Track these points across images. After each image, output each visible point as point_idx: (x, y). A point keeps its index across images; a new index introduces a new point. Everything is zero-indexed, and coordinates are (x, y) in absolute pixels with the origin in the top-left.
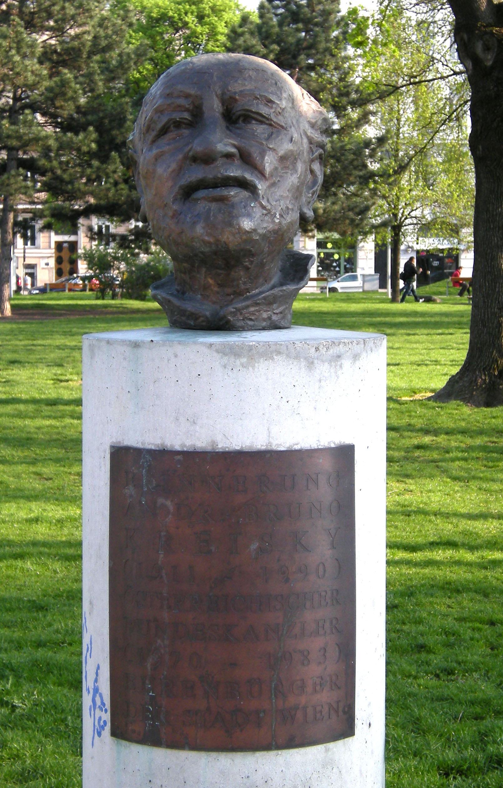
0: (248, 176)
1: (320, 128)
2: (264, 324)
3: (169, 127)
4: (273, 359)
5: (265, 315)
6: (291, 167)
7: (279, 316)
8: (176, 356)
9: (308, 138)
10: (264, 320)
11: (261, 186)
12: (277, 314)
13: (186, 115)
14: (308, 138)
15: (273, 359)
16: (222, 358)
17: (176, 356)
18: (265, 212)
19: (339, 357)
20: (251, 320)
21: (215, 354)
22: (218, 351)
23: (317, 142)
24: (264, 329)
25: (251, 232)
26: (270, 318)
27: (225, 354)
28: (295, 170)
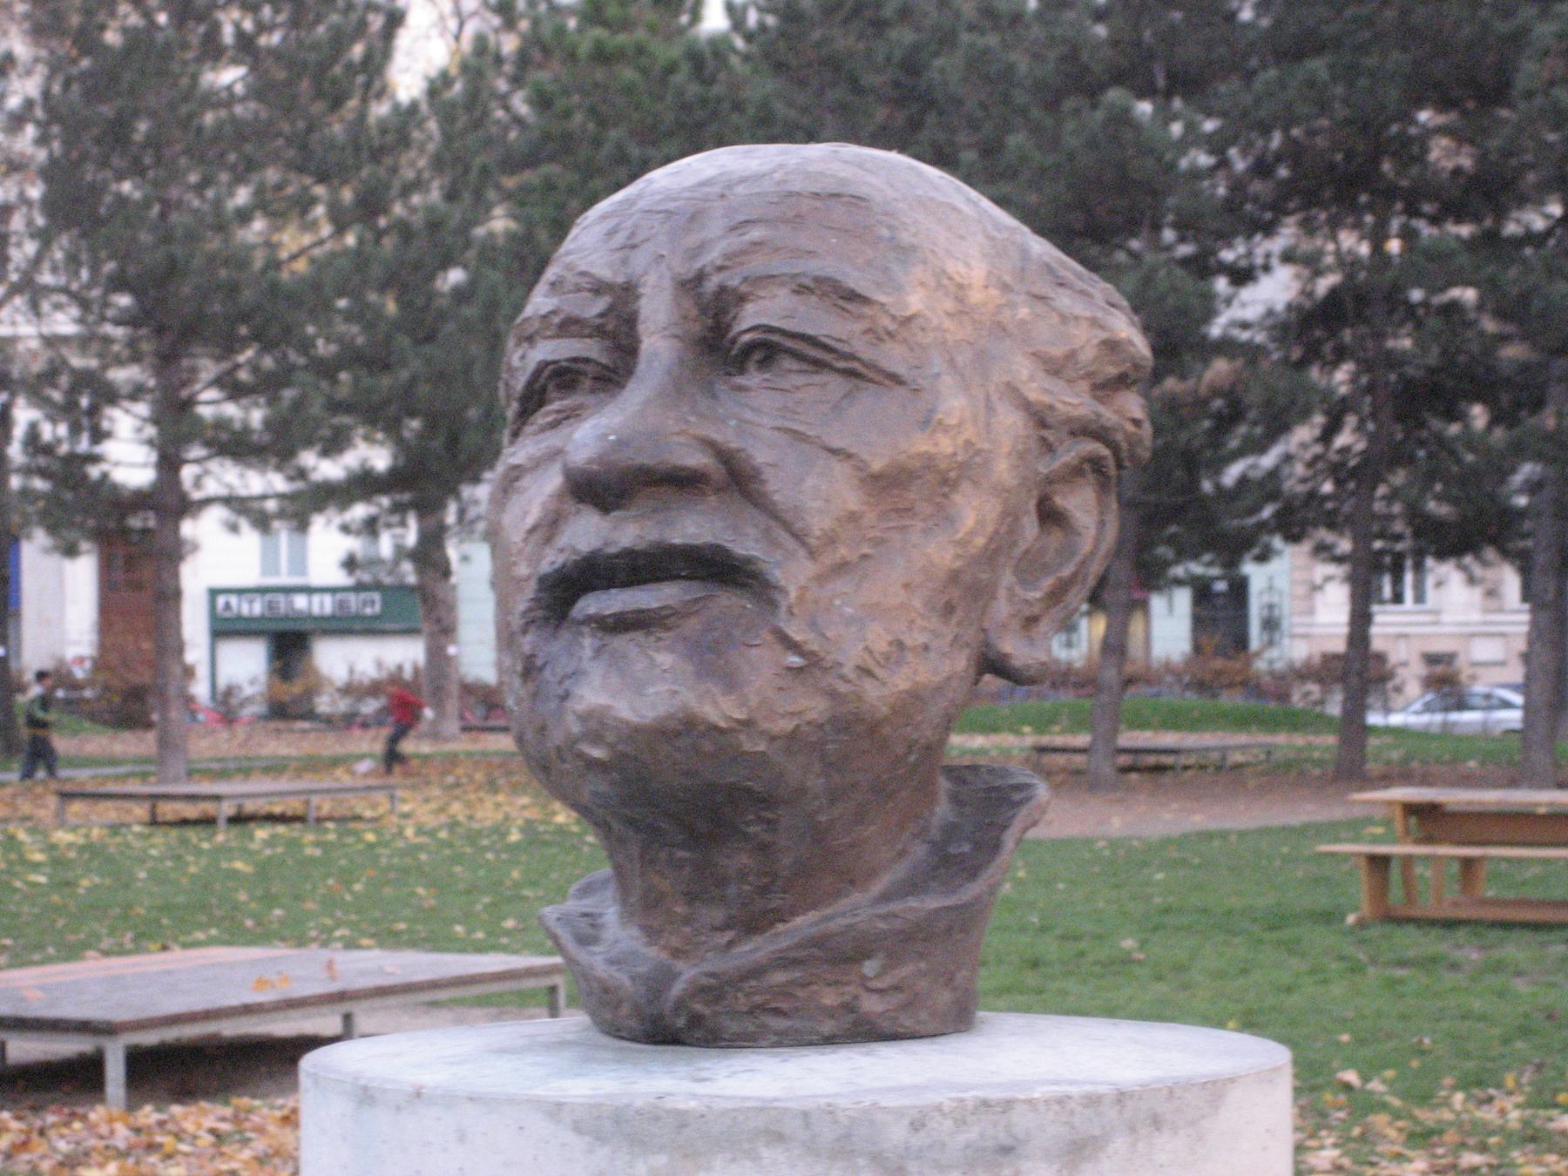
0: (746, 544)
1: (1089, 375)
2: (827, 1027)
3: (544, 390)
4: (756, 1158)
5: (829, 998)
6: (924, 508)
7: (896, 999)
8: (462, 1138)
9: (1027, 406)
10: (830, 1013)
11: (792, 574)
12: (881, 991)
13: (591, 348)
14: (1027, 406)
15: (756, 1158)
16: (591, 1151)
17: (462, 1138)
18: (795, 660)
19: (1006, 1150)
20: (778, 1012)
21: (570, 1137)
22: (578, 1128)
23: (1069, 420)
24: (830, 1041)
25: (731, 730)
26: (848, 1007)
27: (600, 1138)
28: (944, 517)
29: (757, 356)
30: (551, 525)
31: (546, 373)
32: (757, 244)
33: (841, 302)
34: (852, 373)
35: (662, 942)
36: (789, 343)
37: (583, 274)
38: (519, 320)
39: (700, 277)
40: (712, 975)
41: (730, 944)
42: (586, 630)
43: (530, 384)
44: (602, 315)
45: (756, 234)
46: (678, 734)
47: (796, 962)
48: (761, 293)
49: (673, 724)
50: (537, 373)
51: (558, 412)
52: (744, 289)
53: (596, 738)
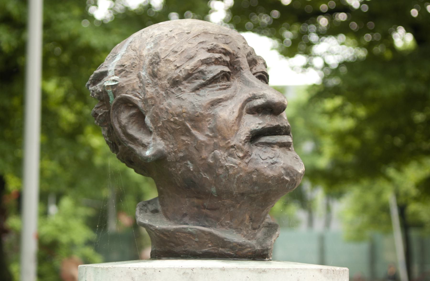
35: (242, 233)
42: (276, 146)
51: (227, 85)
53: (288, 174)
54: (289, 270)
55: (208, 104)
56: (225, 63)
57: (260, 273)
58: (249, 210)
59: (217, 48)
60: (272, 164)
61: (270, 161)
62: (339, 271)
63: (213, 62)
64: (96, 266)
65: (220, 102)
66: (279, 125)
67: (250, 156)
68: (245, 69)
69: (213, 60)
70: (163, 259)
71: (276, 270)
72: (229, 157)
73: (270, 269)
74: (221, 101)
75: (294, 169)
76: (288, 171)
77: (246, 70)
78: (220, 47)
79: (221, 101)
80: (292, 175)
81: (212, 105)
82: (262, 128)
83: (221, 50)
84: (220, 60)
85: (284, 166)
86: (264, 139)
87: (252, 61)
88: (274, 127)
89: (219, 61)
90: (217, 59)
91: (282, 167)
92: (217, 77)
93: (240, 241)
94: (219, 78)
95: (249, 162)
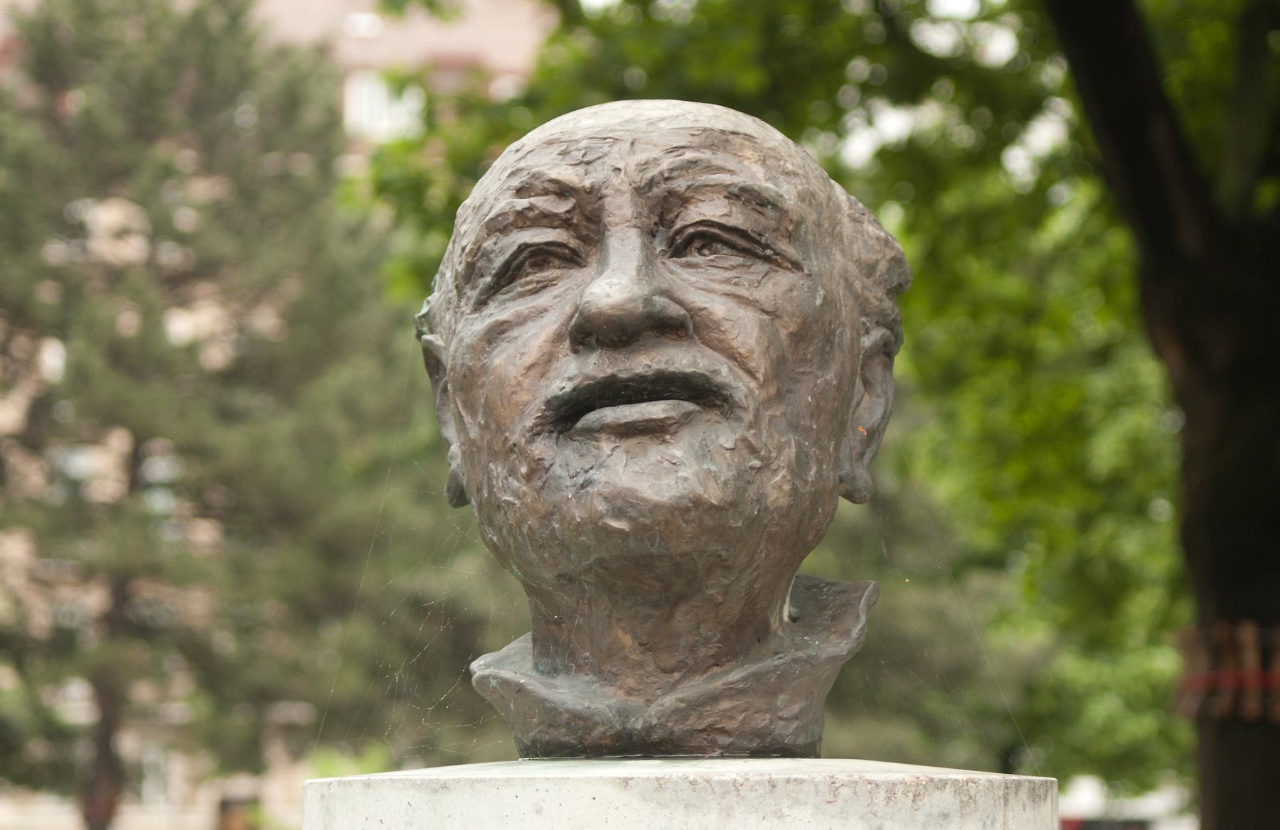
29: (697, 244)
30: (544, 365)
31: (525, 254)
32: (694, 163)
33: (759, 208)
34: (767, 259)
35: (619, 683)
36: (725, 236)
37: (552, 181)
38: (833, 182)
39: (652, 183)
40: (682, 700)
41: (678, 682)
42: (603, 436)
43: (507, 264)
44: (568, 212)
45: (689, 155)
46: (688, 510)
47: (740, 692)
48: (698, 197)
49: (686, 502)
50: (516, 255)
51: (538, 282)
52: (688, 194)
53: (619, 513)
54: (508, 781)
55: (481, 340)
56: (565, 223)
57: (435, 791)
58: (620, 620)
59: (537, 183)
60: (583, 486)
61: (580, 480)
62: (891, 788)
63: (511, 224)
64: (443, 777)
65: (503, 332)
66: (613, 376)
67: (547, 470)
68: (617, 224)
69: (511, 218)
70: (676, 758)
71: (473, 782)
72: (510, 479)
73: (458, 781)
74: (504, 327)
75: (637, 498)
76: (619, 503)
77: (618, 228)
78: (544, 178)
79: (504, 327)
80: (634, 514)
81: (489, 342)
82: (574, 390)
83: (546, 185)
84: (531, 214)
85: (606, 491)
86: (592, 418)
87: (665, 197)
88: (599, 383)
89: (529, 219)
90: (520, 214)
91: (600, 494)
92: (516, 263)
93: (579, 707)
94: (522, 263)
95: (542, 488)
